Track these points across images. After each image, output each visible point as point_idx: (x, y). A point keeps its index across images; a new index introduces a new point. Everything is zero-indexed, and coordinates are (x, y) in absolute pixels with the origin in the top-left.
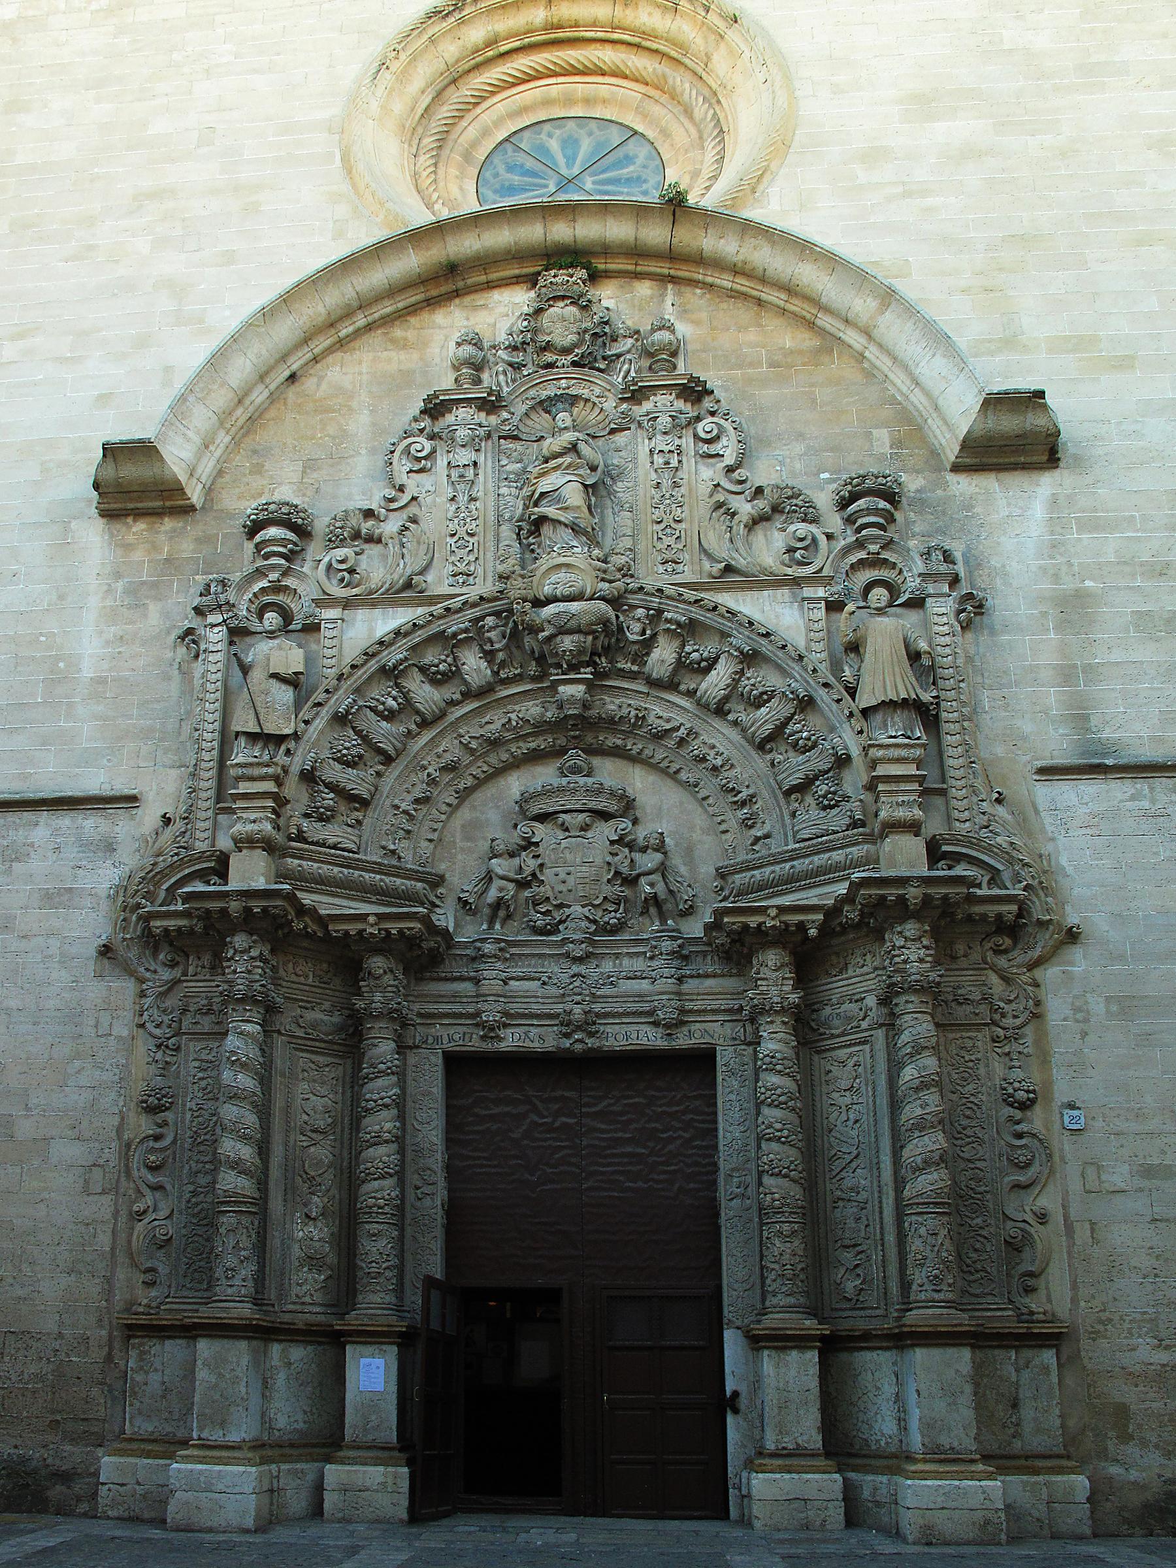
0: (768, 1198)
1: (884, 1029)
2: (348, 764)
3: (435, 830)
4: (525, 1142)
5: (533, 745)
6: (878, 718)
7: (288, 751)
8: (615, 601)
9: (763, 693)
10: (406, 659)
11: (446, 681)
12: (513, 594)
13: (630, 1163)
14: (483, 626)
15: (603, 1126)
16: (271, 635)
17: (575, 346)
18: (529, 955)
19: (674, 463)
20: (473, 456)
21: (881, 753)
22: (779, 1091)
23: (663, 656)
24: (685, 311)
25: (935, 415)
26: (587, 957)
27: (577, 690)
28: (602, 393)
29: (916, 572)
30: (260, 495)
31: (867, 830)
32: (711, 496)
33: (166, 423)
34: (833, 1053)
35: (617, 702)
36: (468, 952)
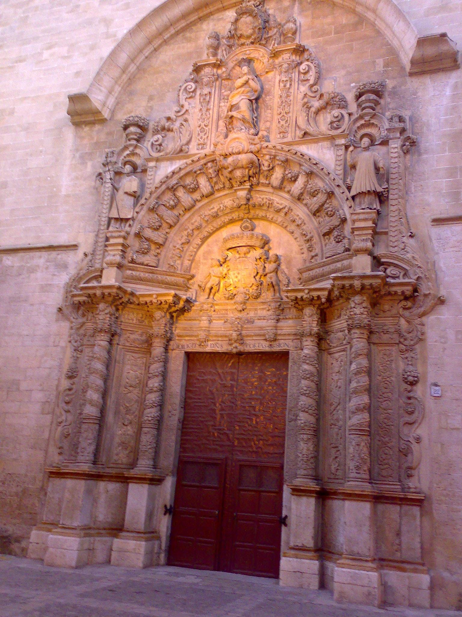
5: (231, 218)
8: (256, 153)
10: (177, 184)
11: (195, 192)
12: (217, 153)
16: (128, 175)
17: (252, 35)
19: (288, 86)
22: (307, 372)
23: (278, 174)
29: (385, 128)
30: (131, 112)
32: (303, 99)
33: (92, 85)
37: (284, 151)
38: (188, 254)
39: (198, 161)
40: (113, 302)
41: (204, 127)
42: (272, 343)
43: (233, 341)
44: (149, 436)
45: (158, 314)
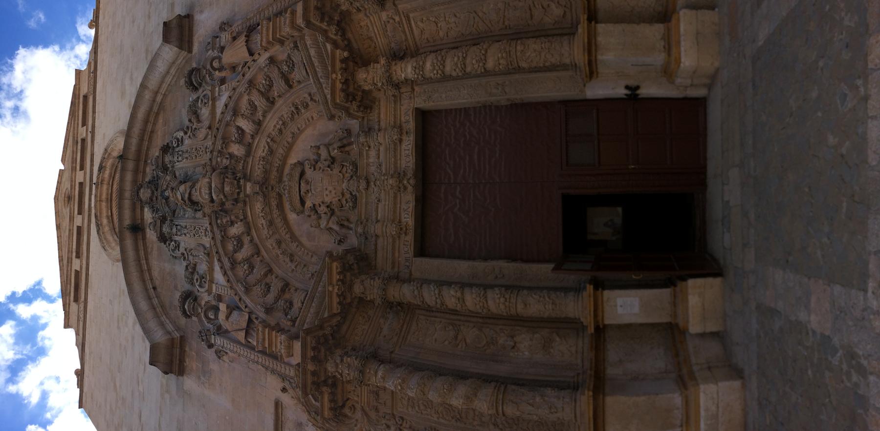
2: (269, 291)
6: (253, 46)
22: (435, 61)
23: (236, 150)
27: (249, 185)
34: (417, 38)
43: (401, 185)
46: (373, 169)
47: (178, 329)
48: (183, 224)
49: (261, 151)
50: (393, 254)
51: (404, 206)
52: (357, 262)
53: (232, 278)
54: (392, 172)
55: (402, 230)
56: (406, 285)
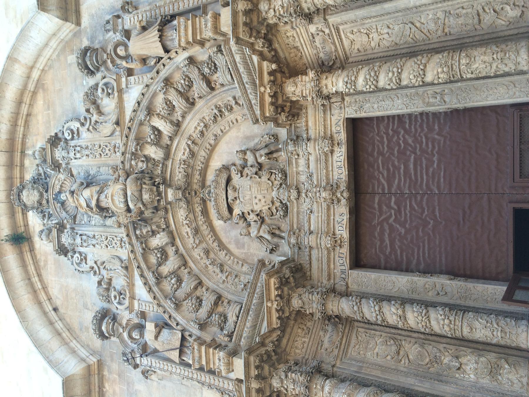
0: (441, 76)
1: (327, 17)
2: (200, 305)
3: (238, 262)
4: (407, 226)
5: (200, 213)
6: (168, 43)
7: (189, 335)
9: (166, 104)
11: (167, 253)
13: (421, 166)
14: (141, 235)
15: (396, 181)
17: (39, 191)
18: (298, 219)
20: (78, 236)
21: (183, 40)
22: (368, 77)
23: (154, 152)
24: (33, 146)
25: (58, 36)
26: (298, 189)
28: (58, 179)
29: (114, 36)
31: (222, 44)
35: (178, 174)
36: (296, 251)
37: (127, 142)
38: (235, 267)
39: (132, 246)
40: (273, 366)
41: (108, 240)
42: (336, 142)
44: (477, 324)
45: (296, 303)
46: (303, 178)
47: (93, 353)
48: (91, 234)
49: (180, 152)
50: (329, 266)
51: (337, 218)
52: (294, 275)
53: (159, 295)
54: (324, 184)
55: (337, 243)
56: (343, 299)
